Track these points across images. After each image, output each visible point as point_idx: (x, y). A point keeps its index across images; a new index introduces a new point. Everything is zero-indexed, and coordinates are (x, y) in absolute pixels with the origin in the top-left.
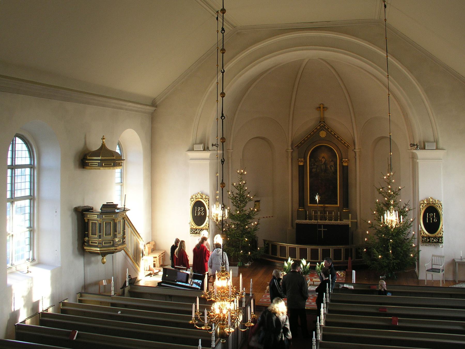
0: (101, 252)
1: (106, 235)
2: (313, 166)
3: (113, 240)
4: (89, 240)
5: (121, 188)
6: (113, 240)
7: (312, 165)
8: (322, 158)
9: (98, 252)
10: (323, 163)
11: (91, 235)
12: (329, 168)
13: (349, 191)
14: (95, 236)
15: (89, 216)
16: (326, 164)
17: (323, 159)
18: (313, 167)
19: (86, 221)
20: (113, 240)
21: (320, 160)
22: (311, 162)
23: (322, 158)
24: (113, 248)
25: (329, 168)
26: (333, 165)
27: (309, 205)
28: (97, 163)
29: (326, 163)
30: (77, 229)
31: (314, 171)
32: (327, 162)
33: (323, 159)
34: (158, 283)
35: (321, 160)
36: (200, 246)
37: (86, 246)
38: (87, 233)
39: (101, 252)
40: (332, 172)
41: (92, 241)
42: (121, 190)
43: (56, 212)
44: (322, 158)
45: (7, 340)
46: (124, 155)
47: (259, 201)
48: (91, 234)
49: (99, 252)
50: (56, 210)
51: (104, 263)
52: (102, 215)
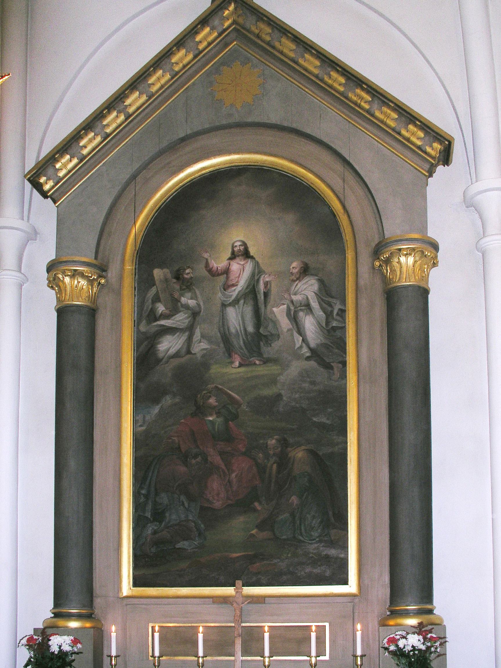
2: (167, 317)
7: (161, 308)
8: (233, 257)
10: (239, 288)
12: (285, 323)
13: (358, 547)
16: (261, 297)
17: (235, 266)
18: (162, 322)
21: (213, 273)
22: (153, 290)
23: (233, 257)
25: (285, 323)
26: (315, 304)
27: (327, 658)
29: (261, 287)
31: (172, 351)
32: (266, 284)
33: (235, 266)
35: (227, 271)
36: (181, 337)
40: (305, 351)
44: (229, 255)
45: (228, 391)
47: (23, 220)
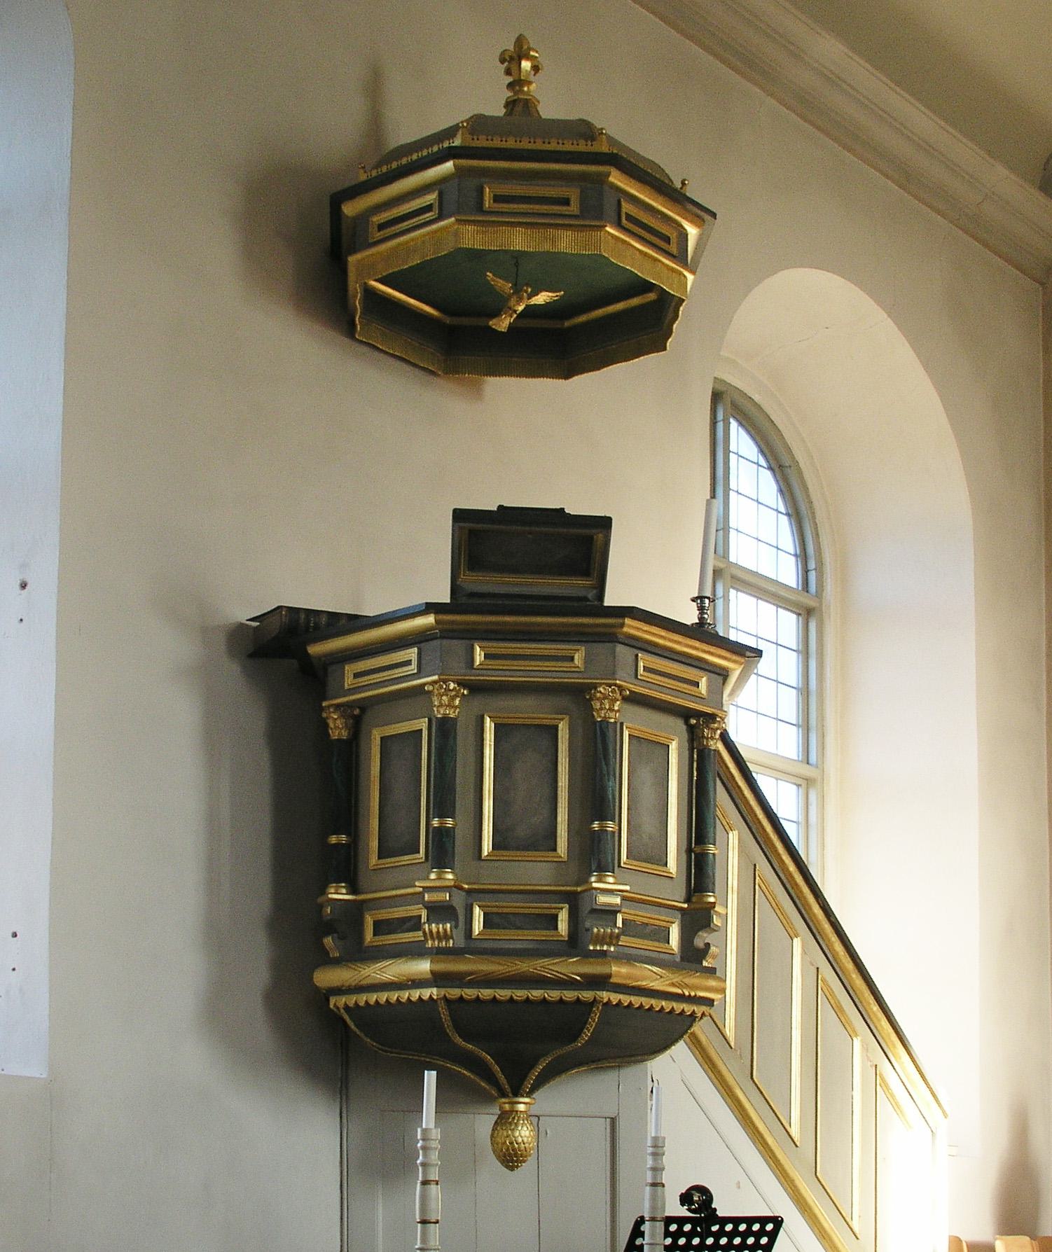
0: (454, 993)
1: (506, 848)
3: (573, 900)
4: (354, 913)
5: (802, 804)
6: (573, 900)
9: (426, 993)
11: (374, 860)
14: (406, 859)
15: (356, 675)
19: (338, 728)
20: (575, 893)
24: (571, 967)
28: (431, 198)
30: (263, 818)
34: (605, 524)
37: (326, 960)
38: (343, 838)
39: (454, 993)
41: (384, 914)
42: (801, 819)
43: (24, 586)
46: (828, 557)
48: (374, 844)
49: (434, 992)
50: (24, 566)
51: (511, 1158)
52: (458, 645)
